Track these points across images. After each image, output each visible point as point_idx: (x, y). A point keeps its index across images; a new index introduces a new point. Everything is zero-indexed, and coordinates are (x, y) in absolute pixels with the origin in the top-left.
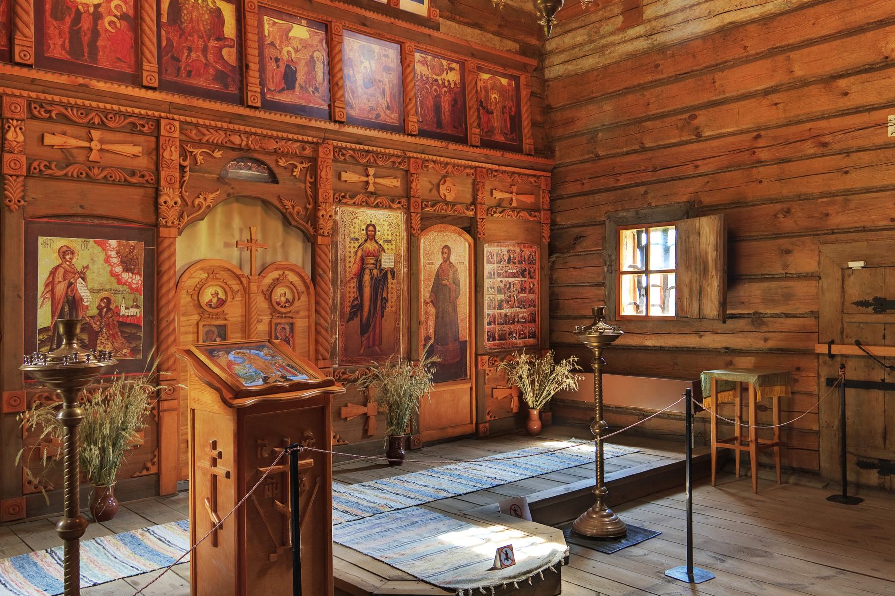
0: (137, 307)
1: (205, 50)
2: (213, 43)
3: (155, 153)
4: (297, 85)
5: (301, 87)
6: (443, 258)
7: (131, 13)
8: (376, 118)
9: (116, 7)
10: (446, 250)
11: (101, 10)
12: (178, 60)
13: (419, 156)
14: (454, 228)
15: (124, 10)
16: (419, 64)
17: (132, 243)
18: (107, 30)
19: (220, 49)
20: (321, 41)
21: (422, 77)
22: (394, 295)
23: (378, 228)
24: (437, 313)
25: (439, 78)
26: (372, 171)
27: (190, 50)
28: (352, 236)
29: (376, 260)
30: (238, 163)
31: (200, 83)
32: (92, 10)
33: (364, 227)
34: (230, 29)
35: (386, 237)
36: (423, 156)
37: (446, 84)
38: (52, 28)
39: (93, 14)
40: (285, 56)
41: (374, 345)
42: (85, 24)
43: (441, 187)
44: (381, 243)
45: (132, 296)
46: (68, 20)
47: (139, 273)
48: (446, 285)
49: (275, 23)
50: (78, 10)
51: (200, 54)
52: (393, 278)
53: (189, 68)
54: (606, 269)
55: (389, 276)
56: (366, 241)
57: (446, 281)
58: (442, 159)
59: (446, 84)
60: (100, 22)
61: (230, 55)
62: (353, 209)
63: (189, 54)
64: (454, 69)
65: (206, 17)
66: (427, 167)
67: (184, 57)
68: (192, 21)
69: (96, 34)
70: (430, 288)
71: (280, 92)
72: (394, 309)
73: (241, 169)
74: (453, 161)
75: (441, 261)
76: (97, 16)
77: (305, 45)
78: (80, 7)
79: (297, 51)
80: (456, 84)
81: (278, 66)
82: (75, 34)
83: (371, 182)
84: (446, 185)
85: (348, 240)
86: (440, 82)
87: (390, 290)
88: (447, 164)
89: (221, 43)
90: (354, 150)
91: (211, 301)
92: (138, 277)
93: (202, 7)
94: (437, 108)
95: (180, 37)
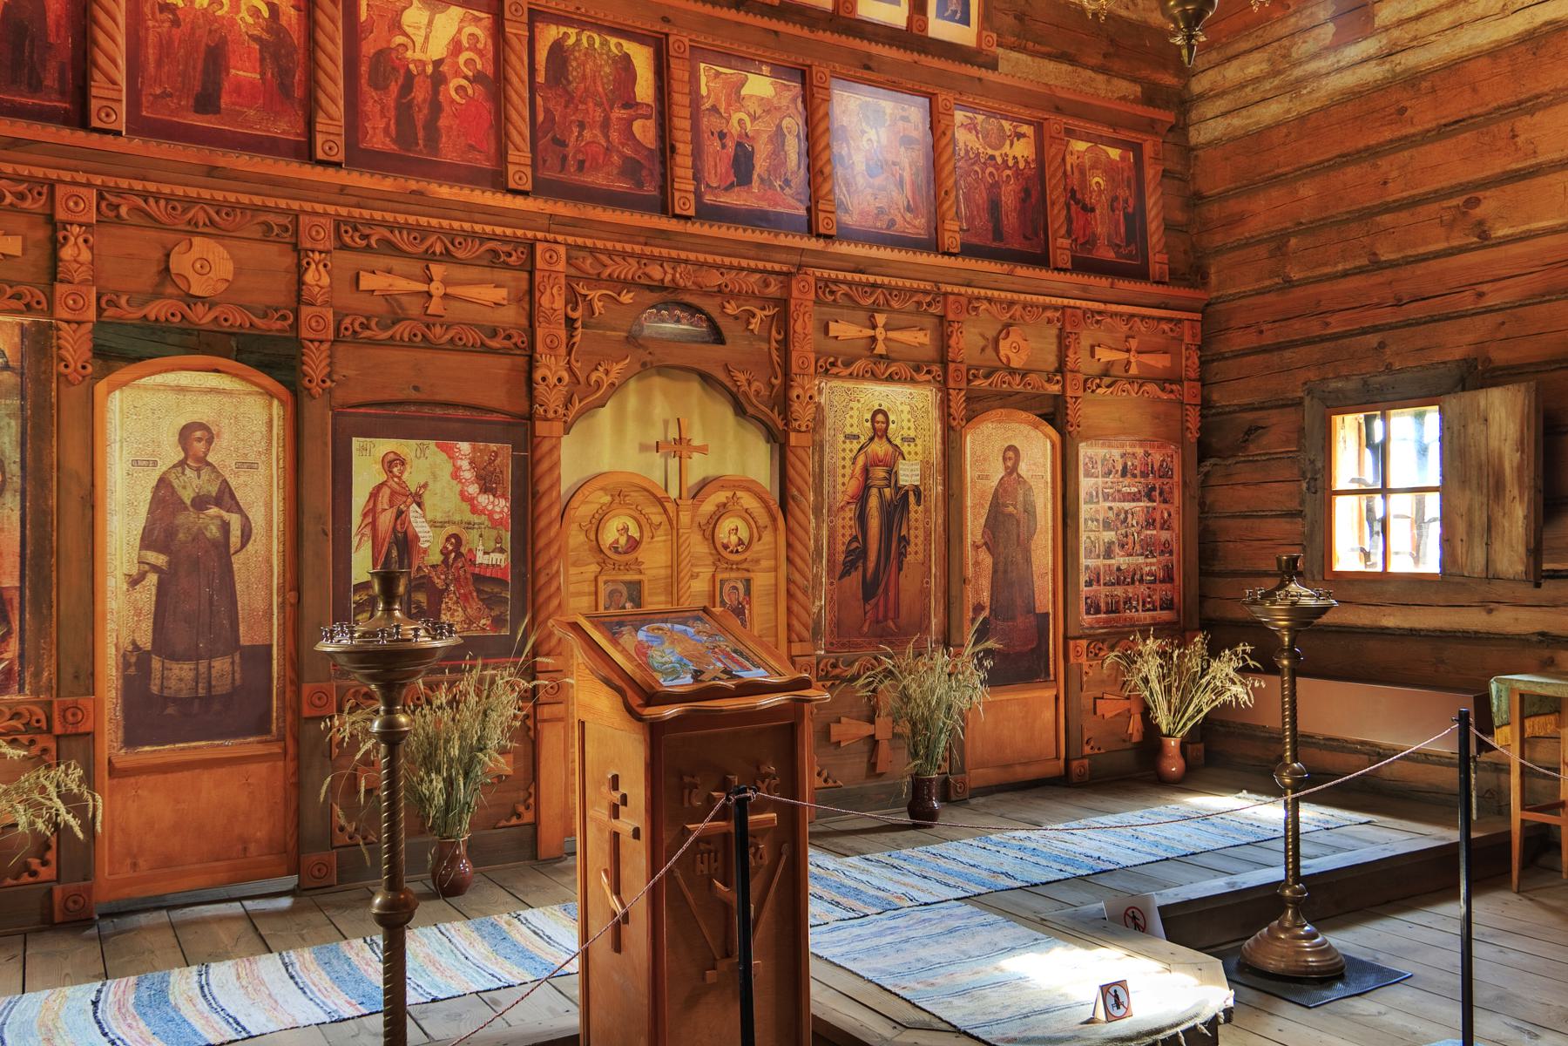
0: (502, 551)
1: (605, 125)
2: (618, 113)
3: (527, 298)
4: (755, 176)
5: (762, 180)
6: (1006, 468)
7: (490, 71)
8: (888, 228)
9: (466, 63)
10: (1011, 454)
11: (444, 68)
12: (563, 144)
13: (963, 290)
14: (1024, 415)
15: (479, 67)
16: (962, 130)
17: (493, 446)
18: (453, 101)
19: (629, 123)
20: (794, 100)
21: (967, 152)
22: (921, 533)
23: (892, 418)
24: (995, 564)
25: (997, 153)
26: (881, 319)
27: (582, 126)
28: (848, 430)
29: (889, 473)
30: (659, 311)
31: (597, 179)
32: (430, 69)
33: (869, 416)
34: (644, 89)
35: (905, 433)
36: (970, 290)
37: (1011, 163)
38: (371, 102)
39: (432, 76)
40: (735, 128)
41: (886, 618)
42: (420, 94)
43: (1002, 343)
44: (898, 442)
45: (494, 533)
46: (394, 89)
47: (503, 496)
48: (1011, 515)
49: (718, 74)
50: (408, 71)
51: (597, 132)
52: (918, 503)
53: (580, 157)
54: (1305, 485)
55: (912, 499)
56: (872, 439)
57: (1011, 509)
58: (1003, 294)
59: (1011, 163)
60: (442, 88)
61: (644, 131)
62: (849, 384)
63: (580, 134)
64: (1024, 135)
65: (607, 70)
66: (976, 309)
67: (573, 139)
68: (584, 77)
69: (436, 107)
70: (983, 521)
71: (726, 189)
72: (920, 556)
73: (663, 321)
74: (1022, 297)
75: (1001, 473)
76: (438, 79)
77: (769, 108)
78: (412, 66)
79: (754, 118)
80: (1027, 162)
81: (724, 146)
82: (404, 110)
83: (880, 338)
84: (1009, 340)
85: (841, 438)
86: (999, 160)
87: (912, 523)
88: (1012, 303)
89: (631, 112)
90: (850, 284)
91: (617, 541)
92: (503, 502)
93: (601, 54)
94: (994, 206)
95: (566, 107)
